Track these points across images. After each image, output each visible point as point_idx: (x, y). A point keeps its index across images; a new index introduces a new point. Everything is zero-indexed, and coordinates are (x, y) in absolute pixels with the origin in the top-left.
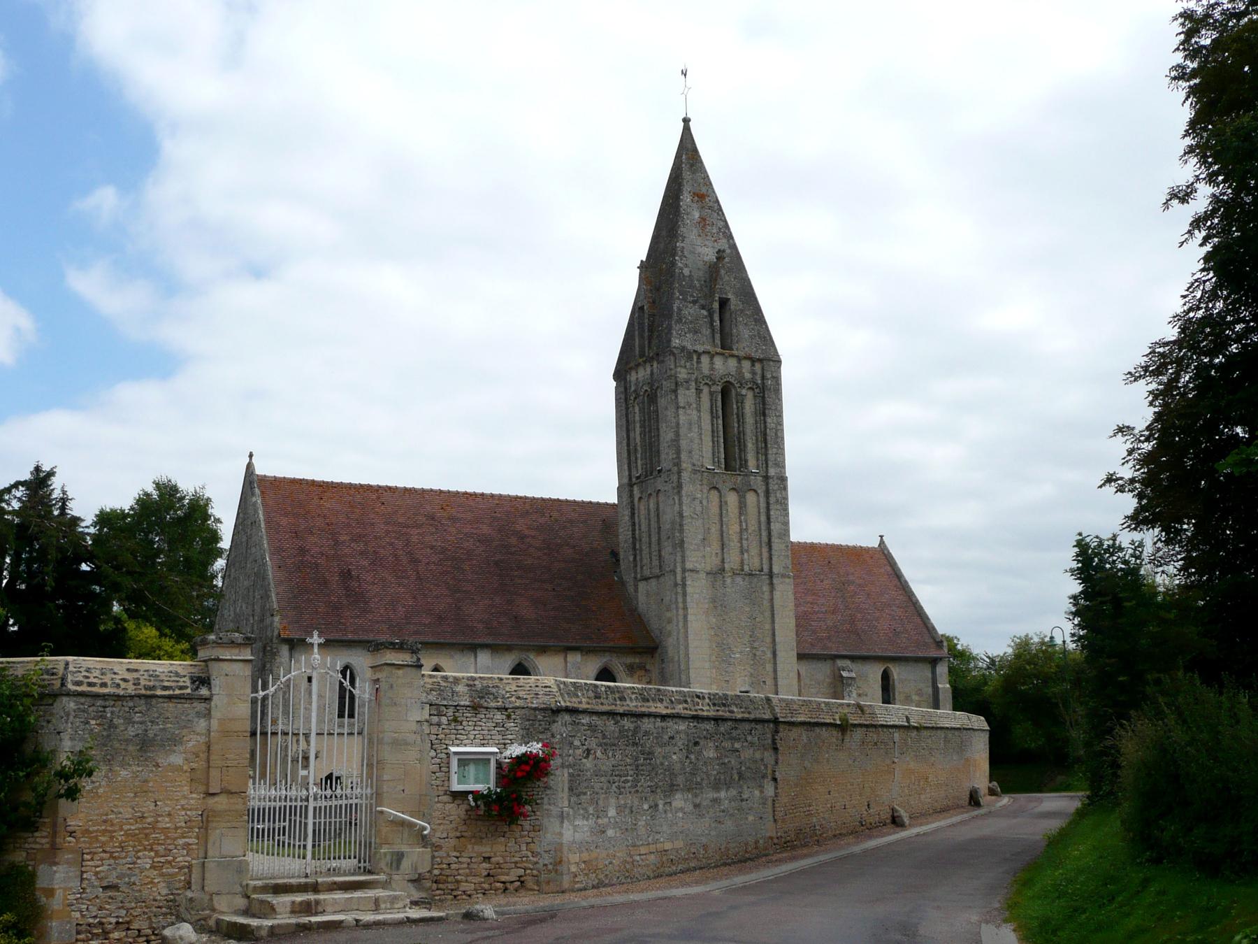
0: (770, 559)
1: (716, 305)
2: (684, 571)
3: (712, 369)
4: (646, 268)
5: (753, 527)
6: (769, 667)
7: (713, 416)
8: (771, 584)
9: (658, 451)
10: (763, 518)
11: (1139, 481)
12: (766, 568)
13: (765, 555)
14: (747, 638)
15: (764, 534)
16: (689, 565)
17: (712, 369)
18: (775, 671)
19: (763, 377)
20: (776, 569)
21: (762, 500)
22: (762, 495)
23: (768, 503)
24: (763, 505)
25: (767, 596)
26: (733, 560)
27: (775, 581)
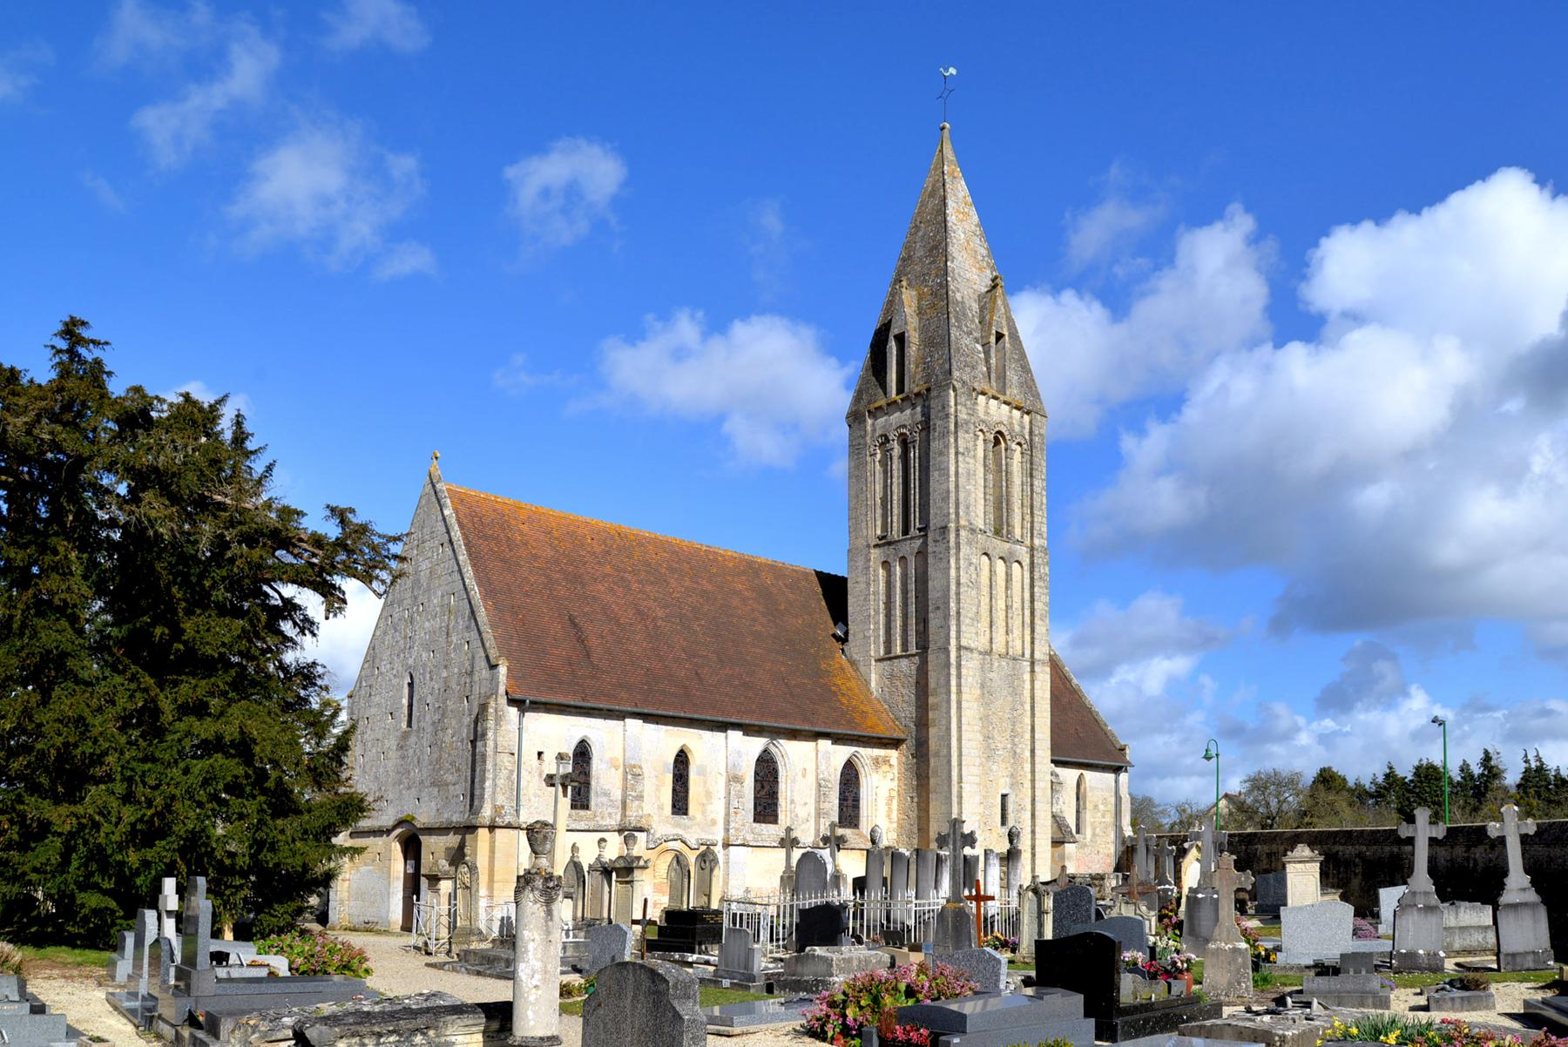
0: (1033, 643)
1: (993, 339)
2: (959, 648)
3: (987, 413)
4: (873, 346)
5: (1017, 605)
6: (1028, 767)
7: (484, 756)
8: (1033, 671)
9: (72, 978)
10: (1027, 595)
11: (210, 715)
12: (1028, 655)
13: (1028, 638)
14: (1008, 733)
15: (1027, 613)
16: (964, 643)
17: (987, 413)
18: (1033, 772)
19: (1031, 432)
20: (1037, 655)
21: (1027, 575)
22: (1026, 568)
23: (1032, 579)
24: (1027, 581)
25: (1028, 686)
26: (999, 646)
27: (1037, 668)
